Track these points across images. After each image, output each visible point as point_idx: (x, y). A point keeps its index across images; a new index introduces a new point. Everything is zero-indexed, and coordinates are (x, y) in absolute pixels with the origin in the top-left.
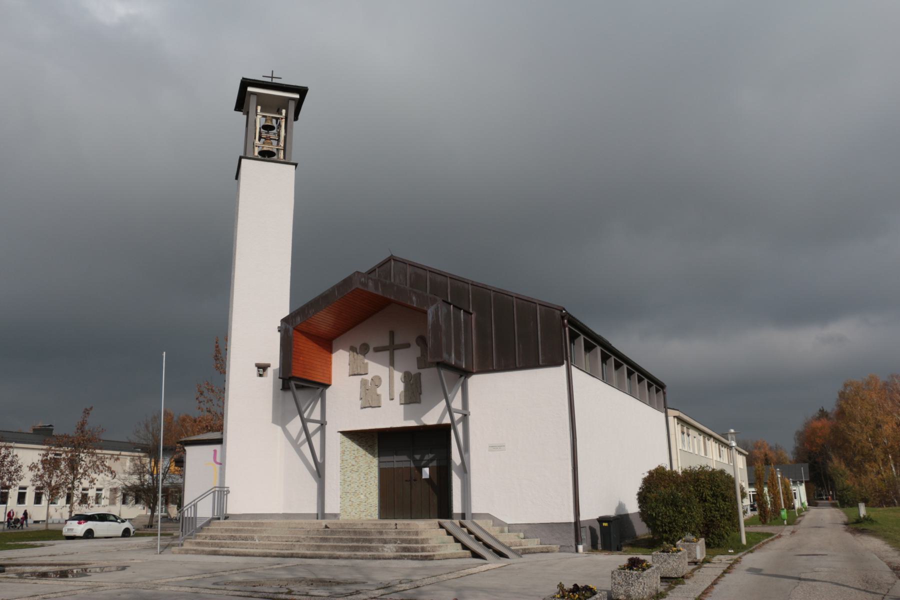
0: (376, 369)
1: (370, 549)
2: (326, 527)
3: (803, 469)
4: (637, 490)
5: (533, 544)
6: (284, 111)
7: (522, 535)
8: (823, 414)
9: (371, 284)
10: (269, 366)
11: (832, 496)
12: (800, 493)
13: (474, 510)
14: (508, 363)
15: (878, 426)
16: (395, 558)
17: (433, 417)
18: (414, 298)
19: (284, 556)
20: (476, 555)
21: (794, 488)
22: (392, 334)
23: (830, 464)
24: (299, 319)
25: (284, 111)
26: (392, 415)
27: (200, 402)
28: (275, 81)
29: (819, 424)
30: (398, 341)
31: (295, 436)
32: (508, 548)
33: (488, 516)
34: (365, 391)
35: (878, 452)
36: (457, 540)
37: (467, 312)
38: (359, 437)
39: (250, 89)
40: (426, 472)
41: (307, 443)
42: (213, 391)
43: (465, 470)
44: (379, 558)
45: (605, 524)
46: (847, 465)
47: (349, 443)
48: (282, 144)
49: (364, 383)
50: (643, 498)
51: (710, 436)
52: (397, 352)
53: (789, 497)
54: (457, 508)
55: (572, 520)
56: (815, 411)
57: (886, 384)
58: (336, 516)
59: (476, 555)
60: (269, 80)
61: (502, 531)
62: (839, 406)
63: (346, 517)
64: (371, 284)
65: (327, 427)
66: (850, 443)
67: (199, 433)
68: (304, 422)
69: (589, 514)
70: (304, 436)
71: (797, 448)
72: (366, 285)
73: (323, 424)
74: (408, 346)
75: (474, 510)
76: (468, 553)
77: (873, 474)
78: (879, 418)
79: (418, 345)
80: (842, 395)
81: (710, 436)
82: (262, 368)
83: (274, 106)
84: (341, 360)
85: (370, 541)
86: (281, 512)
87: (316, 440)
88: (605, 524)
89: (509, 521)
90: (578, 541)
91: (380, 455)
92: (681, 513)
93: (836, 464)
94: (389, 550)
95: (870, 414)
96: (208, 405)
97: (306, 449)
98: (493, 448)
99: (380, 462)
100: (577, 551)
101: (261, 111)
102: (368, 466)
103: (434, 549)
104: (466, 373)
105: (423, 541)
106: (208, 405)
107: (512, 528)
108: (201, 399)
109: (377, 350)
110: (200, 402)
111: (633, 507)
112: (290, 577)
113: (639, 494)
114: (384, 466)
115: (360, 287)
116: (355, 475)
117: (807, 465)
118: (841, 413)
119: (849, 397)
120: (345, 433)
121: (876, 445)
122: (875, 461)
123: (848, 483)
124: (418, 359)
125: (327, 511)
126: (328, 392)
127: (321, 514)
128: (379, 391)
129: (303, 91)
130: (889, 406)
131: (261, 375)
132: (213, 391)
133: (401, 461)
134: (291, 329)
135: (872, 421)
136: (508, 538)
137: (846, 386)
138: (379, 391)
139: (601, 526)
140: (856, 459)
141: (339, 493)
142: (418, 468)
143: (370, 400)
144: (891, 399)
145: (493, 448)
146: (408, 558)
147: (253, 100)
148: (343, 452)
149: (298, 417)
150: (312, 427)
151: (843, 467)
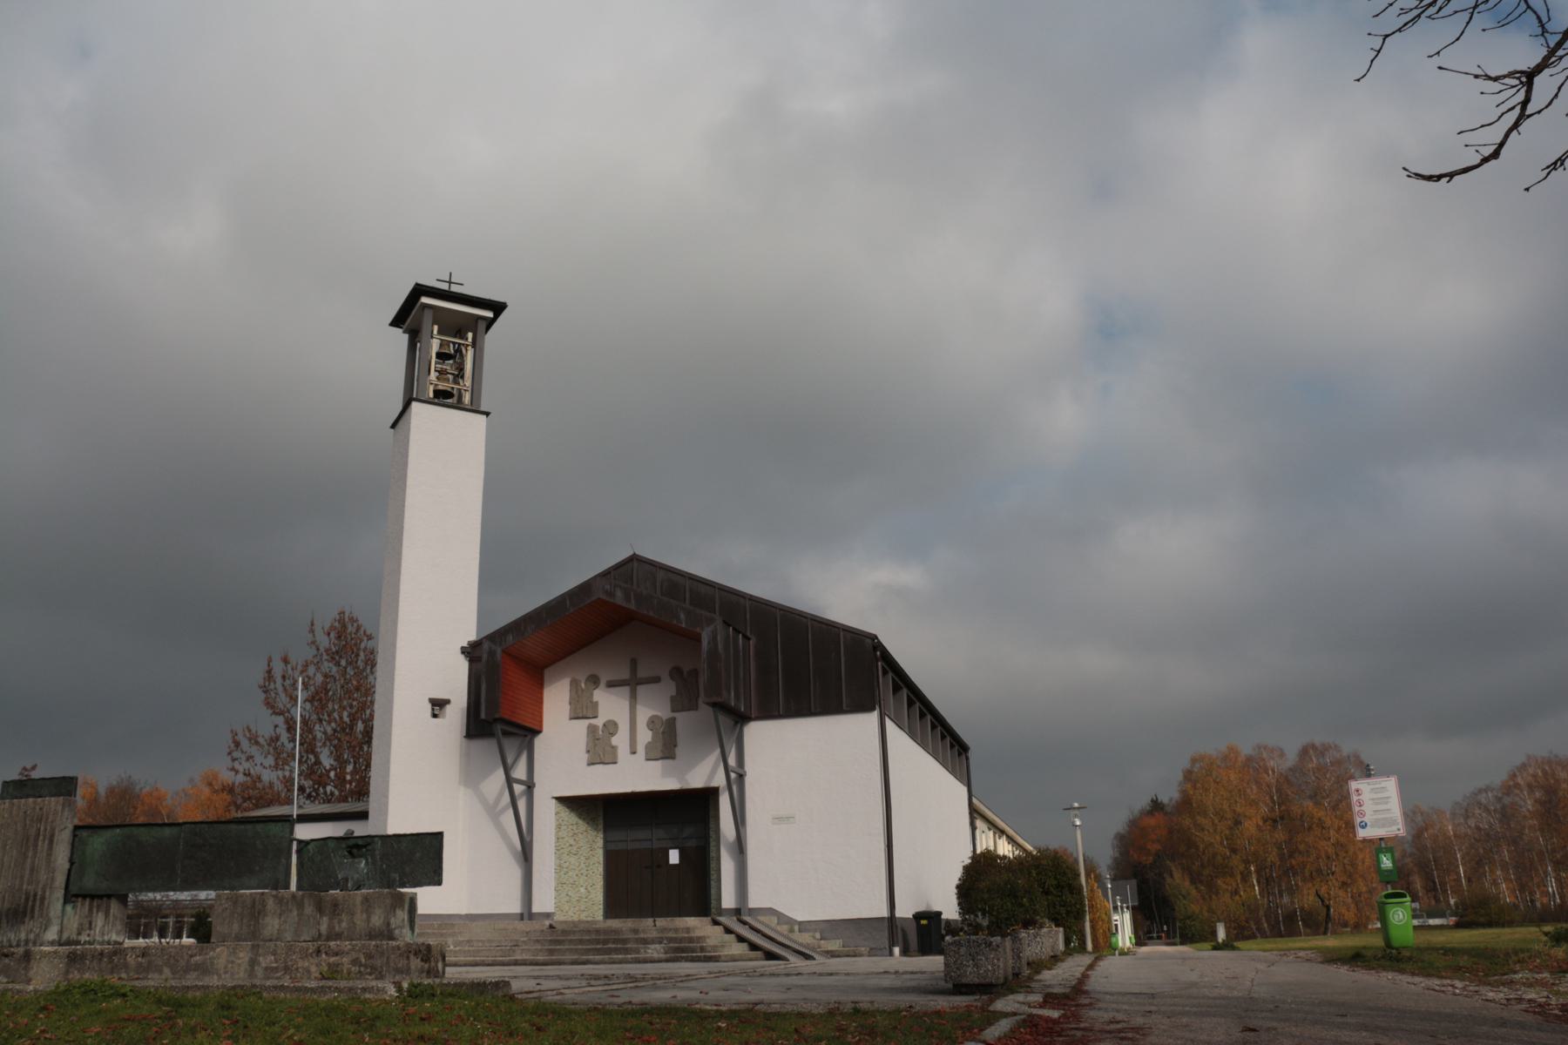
0: (611, 705)
1: (627, 951)
2: (551, 927)
3: (1130, 887)
4: (956, 882)
5: (835, 945)
6: (470, 335)
7: (818, 936)
8: (1156, 806)
9: (619, 593)
10: (448, 702)
11: (1168, 933)
12: (1124, 925)
13: (752, 904)
14: (799, 706)
15: (1237, 823)
16: (667, 961)
17: (702, 773)
18: (682, 616)
19: (503, 964)
20: (771, 956)
21: (1116, 917)
22: (634, 664)
23: (1169, 880)
24: (510, 638)
25: (470, 335)
26: (637, 774)
27: (234, 760)
28: (455, 288)
29: (1152, 821)
30: (642, 673)
31: (491, 798)
32: (814, 949)
33: (771, 911)
34: (596, 740)
35: (1236, 861)
36: (741, 939)
37: (746, 638)
38: (579, 805)
39: (425, 300)
40: (674, 857)
41: (511, 811)
42: (257, 743)
43: (740, 847)
44: (645, 961)
45: (924, 922)
46: (1193, 881)
47: (569, 817)
48: (468, 383)
49: (592, 730)
50: (966, 891)
51: (1002, 832)
52: (641, 689)
53: (1111, 932)
54: (728, 900)
55: (885, 913)
56: (1143, 802)
57: (1249, 759)
58: (548, 915)
59: (771, 956)
60: (445, 286)
61: (792, 931)
62: (1184, 792)
63: (562, 918)
64: (619, 593)
65: (536, 791)
66: (1197, 848)
67: (257, 807)
68: (510, 781)
69: (905, 911)
70: (506, 798)
71: (1115, 859)
72: (611, 594)
73: (530, 786)
74: (657, 680)
75: (752, 904)
76: (759, 954)
77: (1228, 895)
78: (1238, 809)
79: (672, 678)
80: (1188, 775)
81: (1002, 832)
82: (438, 705)
83: (457, 327)
84: (556, 699)
85: (625, 941)
86: (464, 912)
87: (522, 805)
88: (924, 922)
89: (800, 916)
90: (892, 944)
91: (607, 828)
92: (1022, 905)
93: (1177, 881)
94: (655, 951)
95: (1226, 807)
96: (246, 765)
97: (509, 817)
98: (778, 819)
99: (606, 842)
100: (891, 954)
101: (440, 332)
102: (590, 849)
103: (715, 948)
104: (742, 719)
105: (700, 939)
106: (246, 765)
107: (804, 926)
108: (235, 754)
109: (611, 685)
110: (234, 760)
111: (950, 909)
112: (691, 921)
113: (958, 887)
114: (612, 847)
115: (604, 597)
116: (573, 860)
117: (1134, 882)
118: (1185, 804)
119: (1197, 776)
120: (562, 800)
121: (1234, 851)
122: (1232, 875)
123: (1195, 908)
124: (673, 699)
125: (535, 909)
126: (539, 742)
127: (527, 914)
128: (615, 741)
129: (498, 308)
130: (1253, 792)
131: (435, 716)
132: (257, 743)
133: (638, 839)
134: (499, 651)
135: (1229, 815)
136: (805, 939)
137: (1194, 761)
138: (615, 741)
139: (919, 926)
140: (1206, 872)
141: (553, 884)
142: (662, 849)
143: (600, 751)
144: (1257, 782)
145: (778, 819)
146: (687, 960)
147: (428, 317)
148: (559, 827)
149: (500, 773)
150: (518, 788)
151: (1187, 883)
